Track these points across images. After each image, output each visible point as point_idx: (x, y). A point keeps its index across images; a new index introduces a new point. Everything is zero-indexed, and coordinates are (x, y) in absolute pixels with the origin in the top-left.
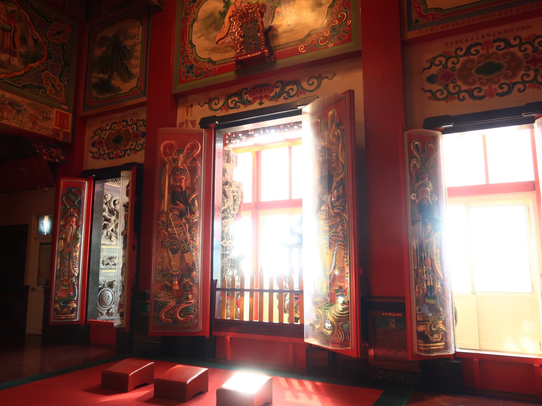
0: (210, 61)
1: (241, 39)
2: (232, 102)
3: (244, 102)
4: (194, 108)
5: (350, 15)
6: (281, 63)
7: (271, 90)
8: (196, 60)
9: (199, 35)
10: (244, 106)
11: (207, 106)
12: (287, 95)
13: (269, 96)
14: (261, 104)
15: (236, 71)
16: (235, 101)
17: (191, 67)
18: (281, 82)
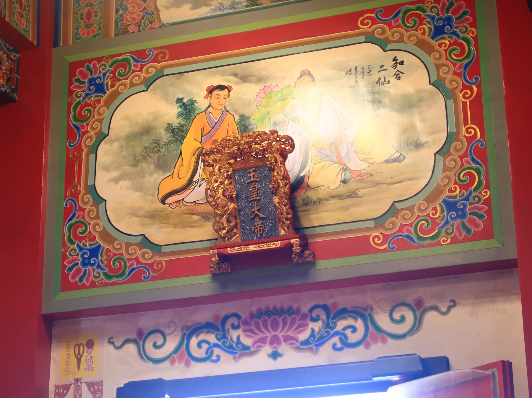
0: (146, 242)
1: (232, 206)
2: (199, 345)
3: (230, 347)
4: (96, 349)
5: (487, 178)
6: (327, 268)
7: (299, 326)
8: (105, 235)
9: (115, 174)
10: (230, 356)
11: (131, 348)
12: (341, 340)
13: (296, 340)
14: (275, 355)
15: (214, 275)
16: (209, 343)
17: (95, 252)
18: (325, 308)
